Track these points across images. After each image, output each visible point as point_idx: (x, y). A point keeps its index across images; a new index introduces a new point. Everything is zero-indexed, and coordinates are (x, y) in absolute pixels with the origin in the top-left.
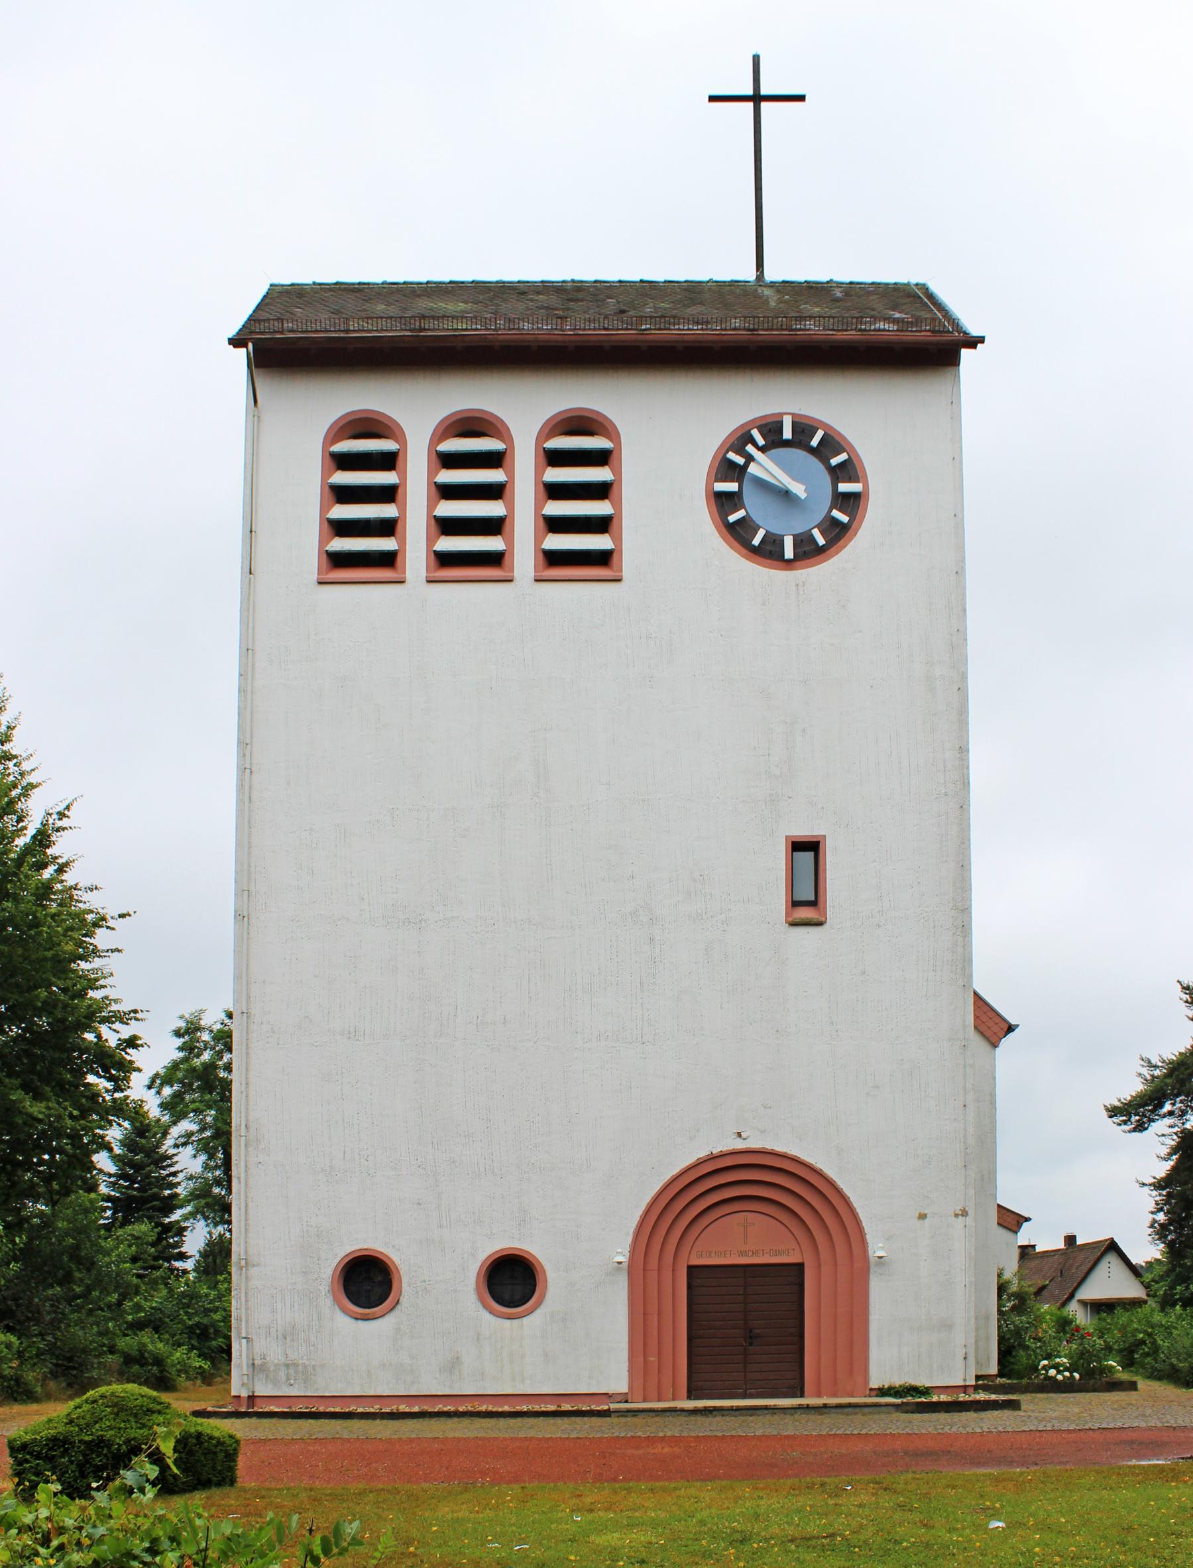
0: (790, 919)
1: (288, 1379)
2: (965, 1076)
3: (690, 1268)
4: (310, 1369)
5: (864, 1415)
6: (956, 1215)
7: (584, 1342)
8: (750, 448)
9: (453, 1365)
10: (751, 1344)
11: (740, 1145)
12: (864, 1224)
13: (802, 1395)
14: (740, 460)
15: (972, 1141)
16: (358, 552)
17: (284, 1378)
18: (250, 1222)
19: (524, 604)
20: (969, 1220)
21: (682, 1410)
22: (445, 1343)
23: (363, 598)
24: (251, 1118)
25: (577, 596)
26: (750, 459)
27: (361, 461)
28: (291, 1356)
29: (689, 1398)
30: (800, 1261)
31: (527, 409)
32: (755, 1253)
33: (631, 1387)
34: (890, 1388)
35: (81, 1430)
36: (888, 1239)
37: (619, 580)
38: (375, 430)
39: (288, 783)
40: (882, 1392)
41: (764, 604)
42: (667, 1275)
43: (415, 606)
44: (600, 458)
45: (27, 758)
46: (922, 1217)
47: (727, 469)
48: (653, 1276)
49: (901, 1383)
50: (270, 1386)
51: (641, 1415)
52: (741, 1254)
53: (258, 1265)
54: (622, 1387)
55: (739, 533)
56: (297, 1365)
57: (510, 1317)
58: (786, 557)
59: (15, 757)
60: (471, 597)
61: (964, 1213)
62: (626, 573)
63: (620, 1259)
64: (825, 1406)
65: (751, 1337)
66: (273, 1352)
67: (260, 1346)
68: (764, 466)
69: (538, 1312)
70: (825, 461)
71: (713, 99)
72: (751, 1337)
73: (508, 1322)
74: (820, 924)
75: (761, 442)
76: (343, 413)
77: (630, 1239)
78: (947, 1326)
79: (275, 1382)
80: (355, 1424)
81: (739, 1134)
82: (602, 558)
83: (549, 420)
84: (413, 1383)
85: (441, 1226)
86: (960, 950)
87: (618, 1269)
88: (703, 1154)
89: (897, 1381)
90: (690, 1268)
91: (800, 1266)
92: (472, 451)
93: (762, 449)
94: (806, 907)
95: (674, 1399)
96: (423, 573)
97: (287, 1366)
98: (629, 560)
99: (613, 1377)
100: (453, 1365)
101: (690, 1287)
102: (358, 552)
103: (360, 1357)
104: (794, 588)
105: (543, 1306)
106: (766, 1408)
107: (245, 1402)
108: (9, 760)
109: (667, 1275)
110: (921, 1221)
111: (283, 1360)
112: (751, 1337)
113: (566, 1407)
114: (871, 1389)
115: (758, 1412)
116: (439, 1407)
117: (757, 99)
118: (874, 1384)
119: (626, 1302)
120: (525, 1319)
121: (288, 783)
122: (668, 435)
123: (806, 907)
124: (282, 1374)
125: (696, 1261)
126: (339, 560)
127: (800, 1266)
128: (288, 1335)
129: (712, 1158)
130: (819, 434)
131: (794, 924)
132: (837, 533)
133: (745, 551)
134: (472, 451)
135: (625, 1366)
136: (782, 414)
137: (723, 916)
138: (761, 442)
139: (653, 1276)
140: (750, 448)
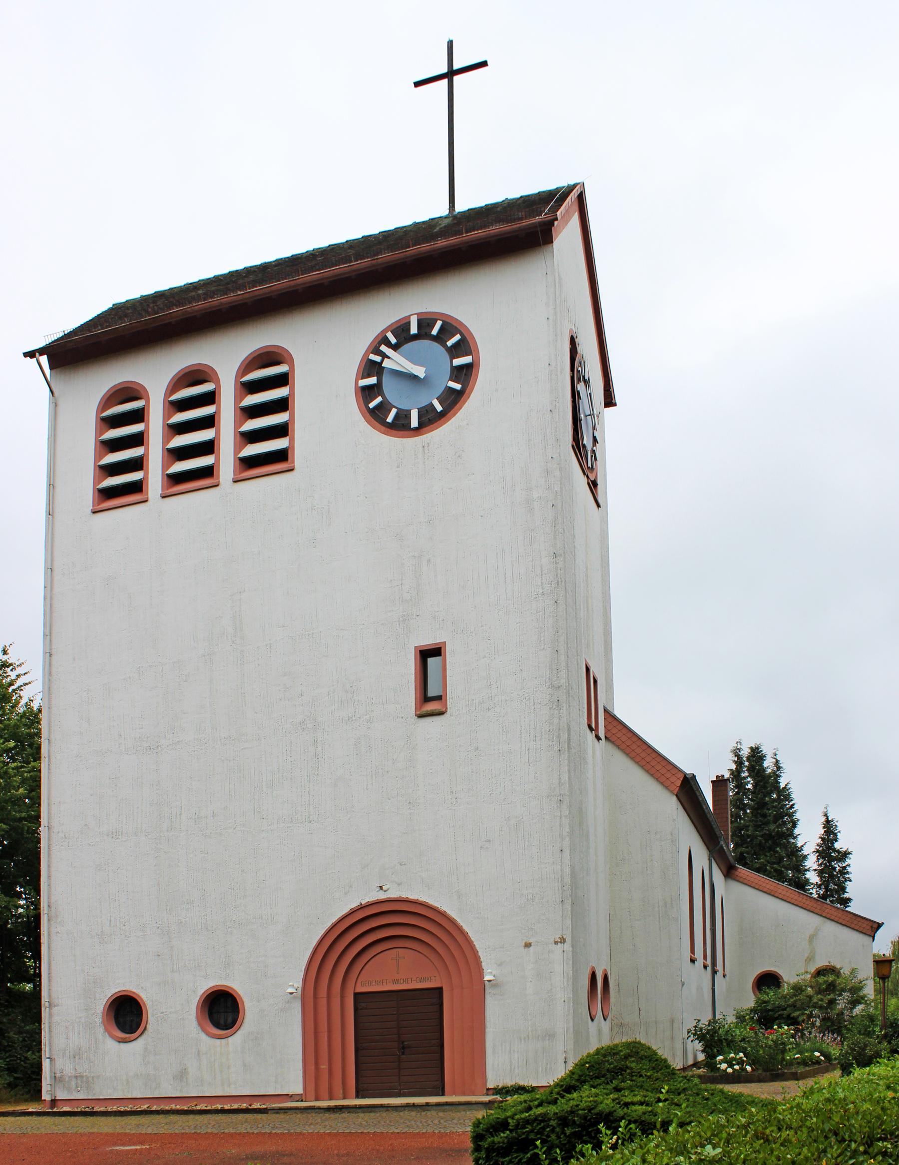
0: (418, 713)
1: (77, 1087)
2: (561, 825)
3: (356, 995)
4: (90, 1079)
5: (444, 1111)
6: (556, 943)
7: (270, 1058)
8: (383, 348)
9: (182, 1075)
10: (403, 1053)
11: (382, 896)
12: (480, 954)
13: (443, 1094)
14: (378, 359)
15: (568, 880)
16: (118, 487)
17: (74, 1087)
18: (53, 975)
19: (233, 501)
20: (567, 946)
21: (319, 1108)
22: (176, 1061)
23: (125, 517)
24: (53, 900)
25: (266, 487)
26: (384, 356)
27: (122, 416)
28: (79, 1071)
29: (357, 1097)
30: (439, 985)
31: (225, 356)
32: (406, 981)
33: (305, 1089)
34: (503, 1088)
35: (857, 1113)
36: (500, 965)
37: (292, 470)
38: (134, 395)
39: (74, 659)
40: (497, 1091)
41: (398, 467)
42: (336, 1001)
43: (161, 514)
44: (282, 380)
45: (20, 665)
46: (528, 945)
47: (371, 368)
48: (323, 1002)
49: (513, 1083)
50: (66, 1092)
51: (290, 1112)
52: (396, 982)
53: (58, 1005)
54: (298, 1089)
55: (377, 416)
56: (82, 1077)
57: (219, 1038)
58: (412, 426)
59: (11, 665)
60: (195, 502)
61: (563, 941)
62: (297, 463)
63: (290, 990)
64: (427, 1104)
65: (403, 1048)
66: (65, 1066)
67: (59, 1064)
68: (395, 361)
69: (239, 1032)
70: (444, 344)
71: (418, 84)
72: (403, 1048)
73: (218, 1041)
74: (441, 713)
75: (393, 341)
76: (107, 389)
77: (302, 975)
78: (550, 1036)
79: (69, 1090)
80: (133, 1120)
81: (381, 887)
82: (281, 456)
83: (244, 360)
84: (156, 1088)
85: (173, 971)
86: (556, 721)
87: (295, 998)
88: (354, 905)
89: (509, 1082)
90: (356, 995)
91: (440, 990)
92: (194, 395)
93: (395, 348)
94: (429, 702)
95: (344, 1098)
96: (231, 476)
97: (76, 1077)
98: (299, 457)
99: (290, 1079)
100: (182, 1075)
101: (356, 1009)
102: (118, 487)
103: (117, 1070)
104: (421, 449)
105: (242, 1028)
106: (382, 1106)
107: (48, 1105)
108: (8, 667)
109: (336, 1001)
110: (526, 949)
111: (74, 1073)
112: (403, 1048)
113: (256, 1106)
114: (488, 1089)
115: (377, 1109)
116: (202, 1107)
117: (451, 74)
118: (490, 1085)
119: (488, 1024)
120: (230, 1039)
121: (74, 659)
122: (326, 351)
123: (429, 702)
124: (73, 1083)
125: (360, 989)
126: (108, 494)
127: (440, 990)
128: (76, 1055)
129: (361, 907)
130: (439, 324)
131: (420, 716)
132: (453, 400)
133: (383, 428)
134: (194, 395)
135: (300, 1073)
136: (409, 317)
137: (368, 716)
138: (393, 341)
139: (323, 1002)
140: (383, 348)
